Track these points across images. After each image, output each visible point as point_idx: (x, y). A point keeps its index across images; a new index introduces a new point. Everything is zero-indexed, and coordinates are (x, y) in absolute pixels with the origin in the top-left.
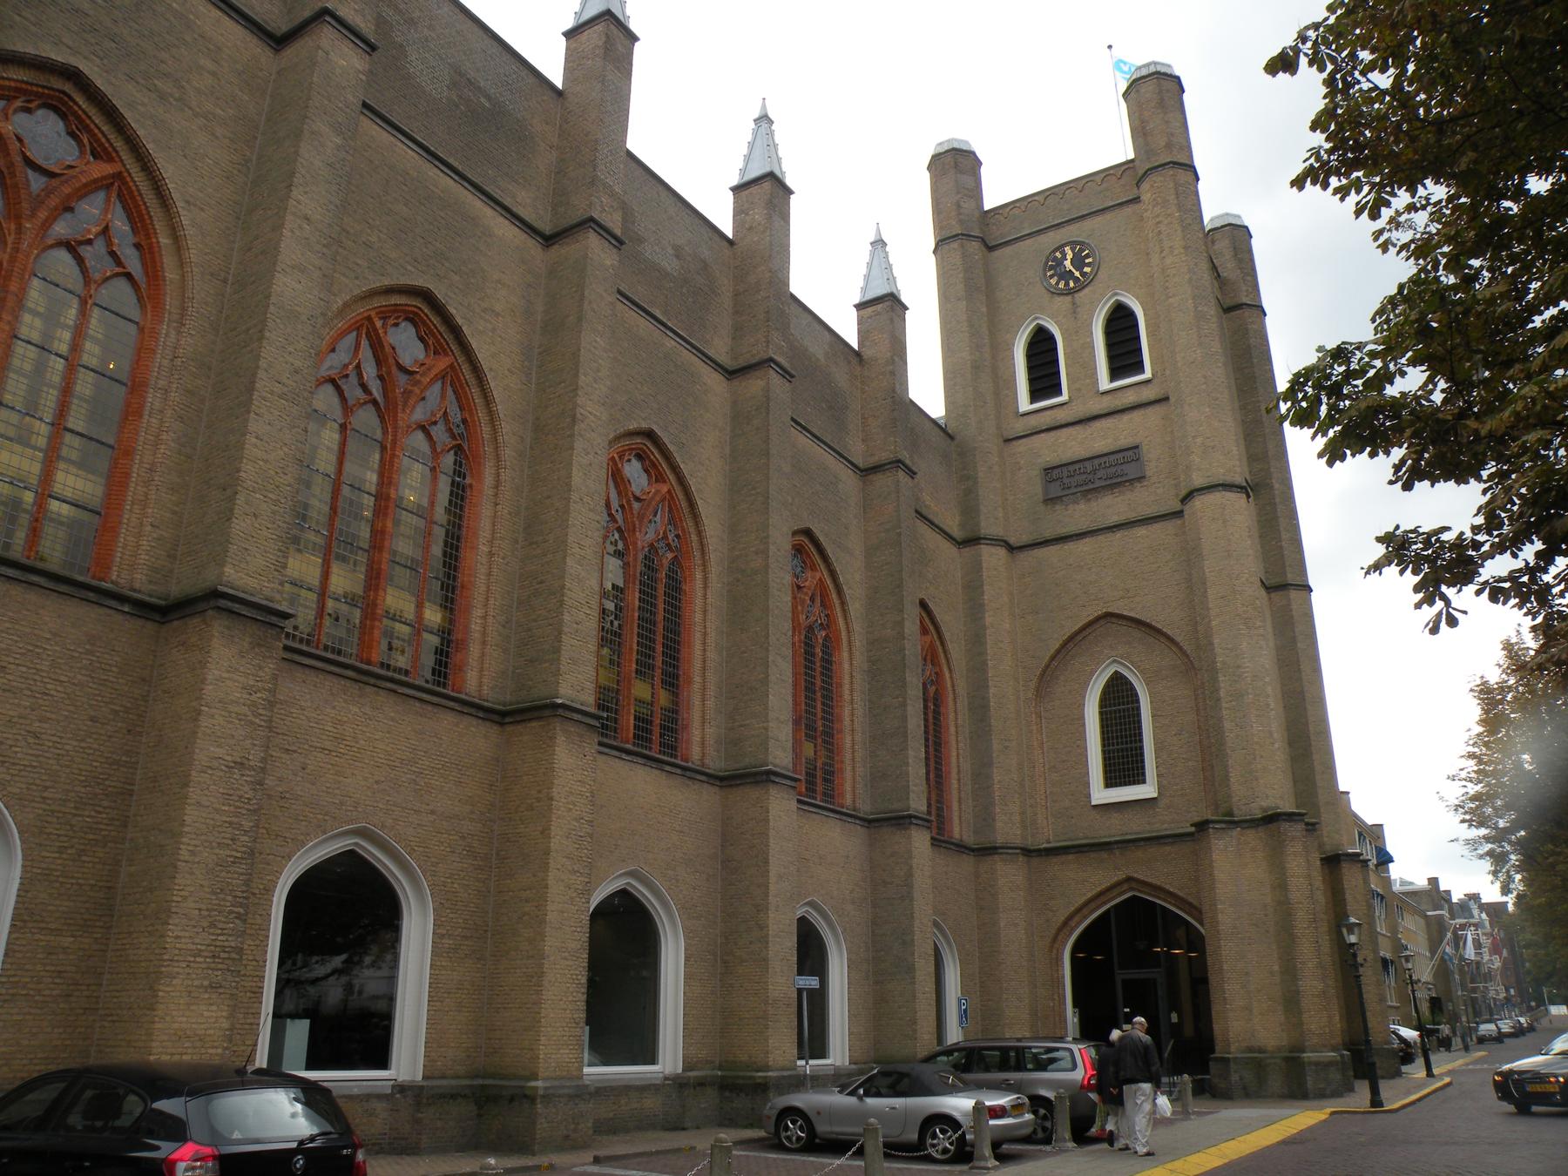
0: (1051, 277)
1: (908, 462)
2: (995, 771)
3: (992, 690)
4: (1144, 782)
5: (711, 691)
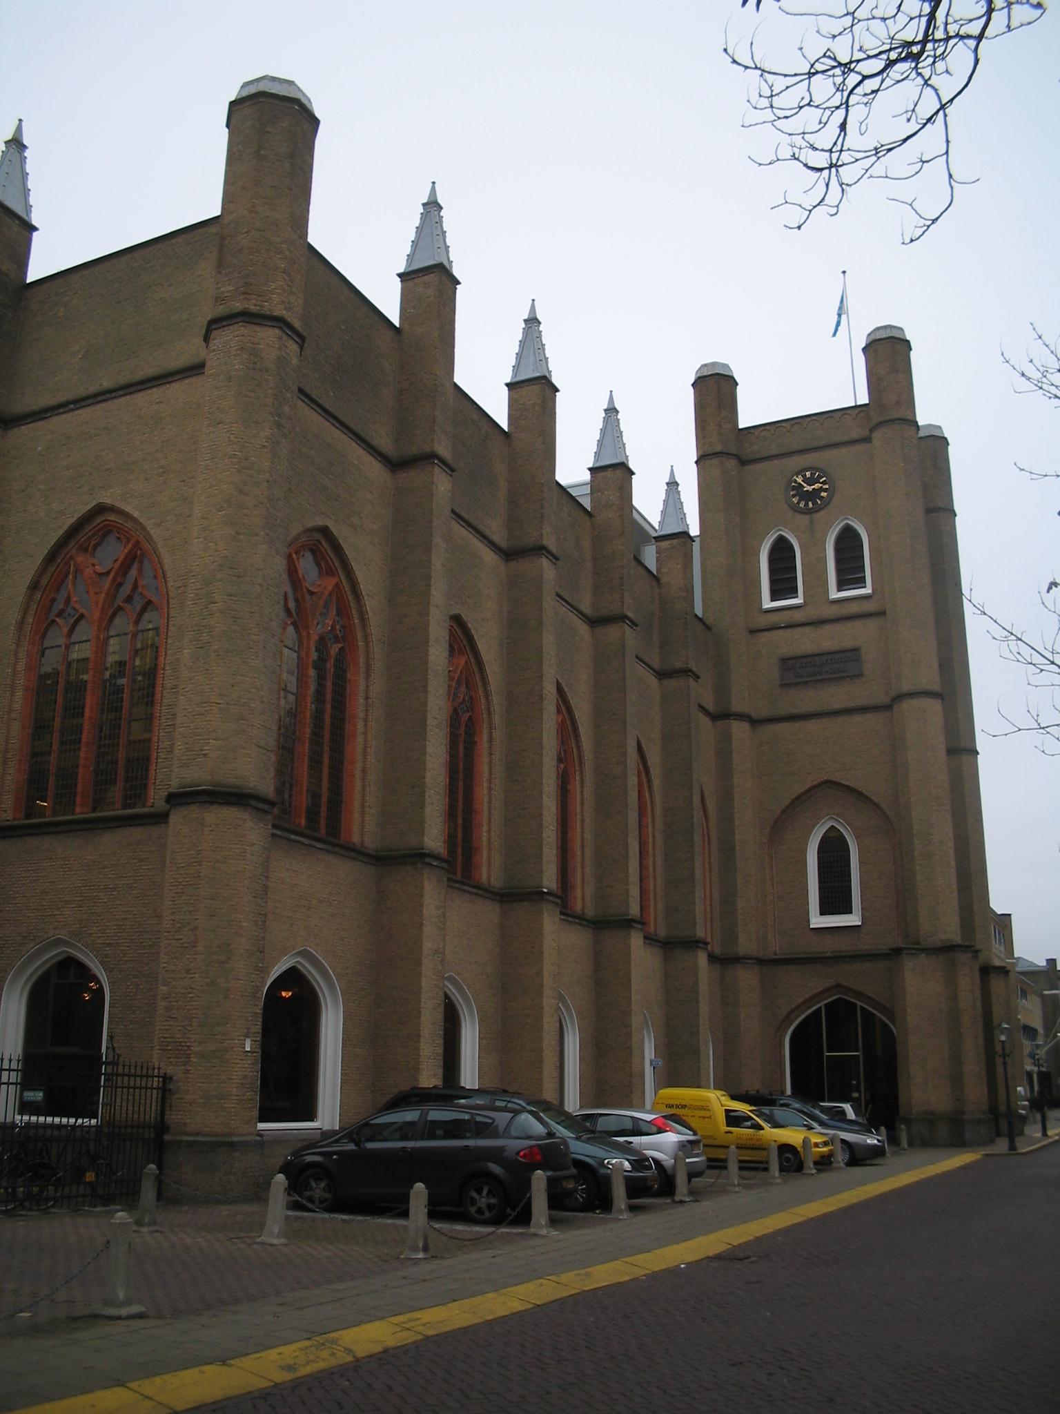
0: (794, 496)
1: (694, 669)
2: (739, 899)
3: (737, 837)
4: (851, 912)
5: (588, 860)
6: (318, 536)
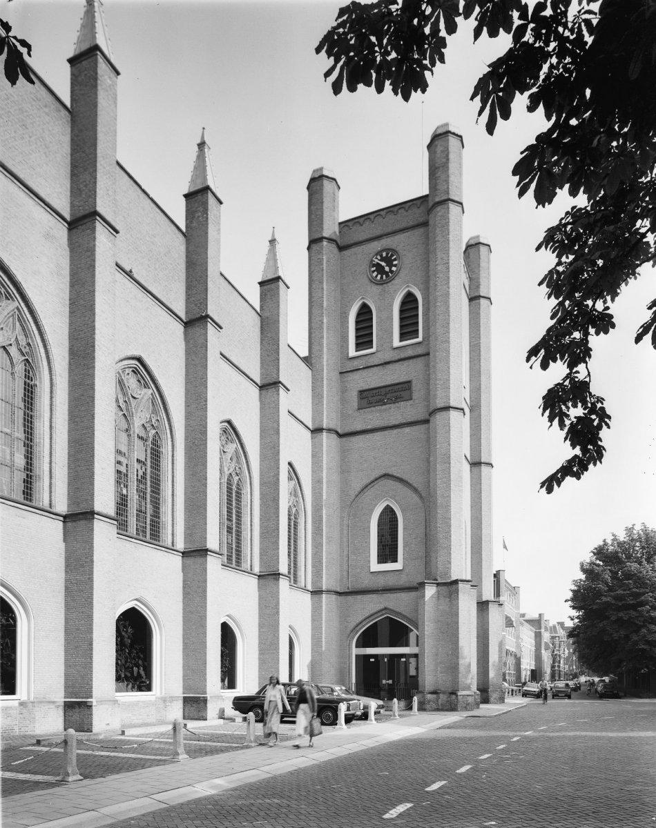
4: (396, 561)
6: (226, 424)
